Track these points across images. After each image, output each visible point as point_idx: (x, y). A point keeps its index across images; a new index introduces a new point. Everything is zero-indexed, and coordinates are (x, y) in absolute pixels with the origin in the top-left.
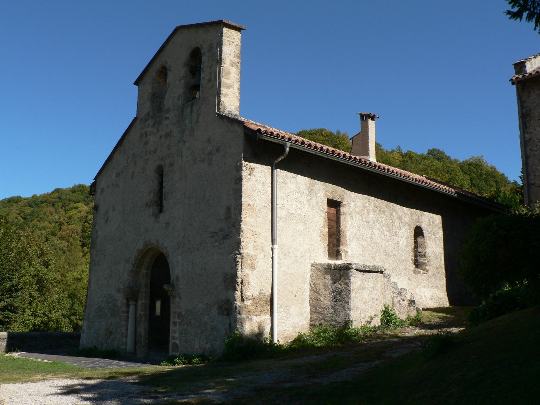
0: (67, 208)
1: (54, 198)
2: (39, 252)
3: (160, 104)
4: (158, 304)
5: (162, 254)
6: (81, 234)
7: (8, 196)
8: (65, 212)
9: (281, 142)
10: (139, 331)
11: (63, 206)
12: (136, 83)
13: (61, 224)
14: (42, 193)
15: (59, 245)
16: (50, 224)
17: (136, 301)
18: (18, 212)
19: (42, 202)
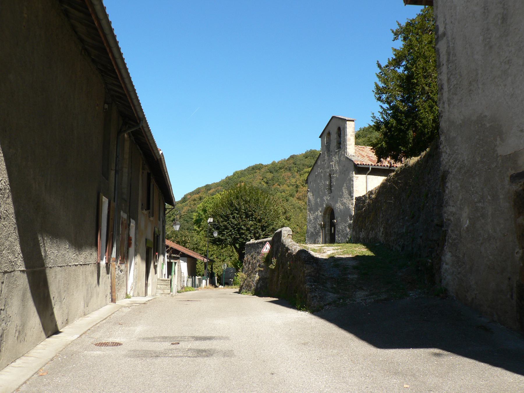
2: (284, 211)
4: (333, 228)
7: (252, 164)
9: (367, 166)
11: (298, 171)
12: (320, 137)
13: (297, 187)
14: (280, 160)
18: (261, 178)
19: (280, 168)
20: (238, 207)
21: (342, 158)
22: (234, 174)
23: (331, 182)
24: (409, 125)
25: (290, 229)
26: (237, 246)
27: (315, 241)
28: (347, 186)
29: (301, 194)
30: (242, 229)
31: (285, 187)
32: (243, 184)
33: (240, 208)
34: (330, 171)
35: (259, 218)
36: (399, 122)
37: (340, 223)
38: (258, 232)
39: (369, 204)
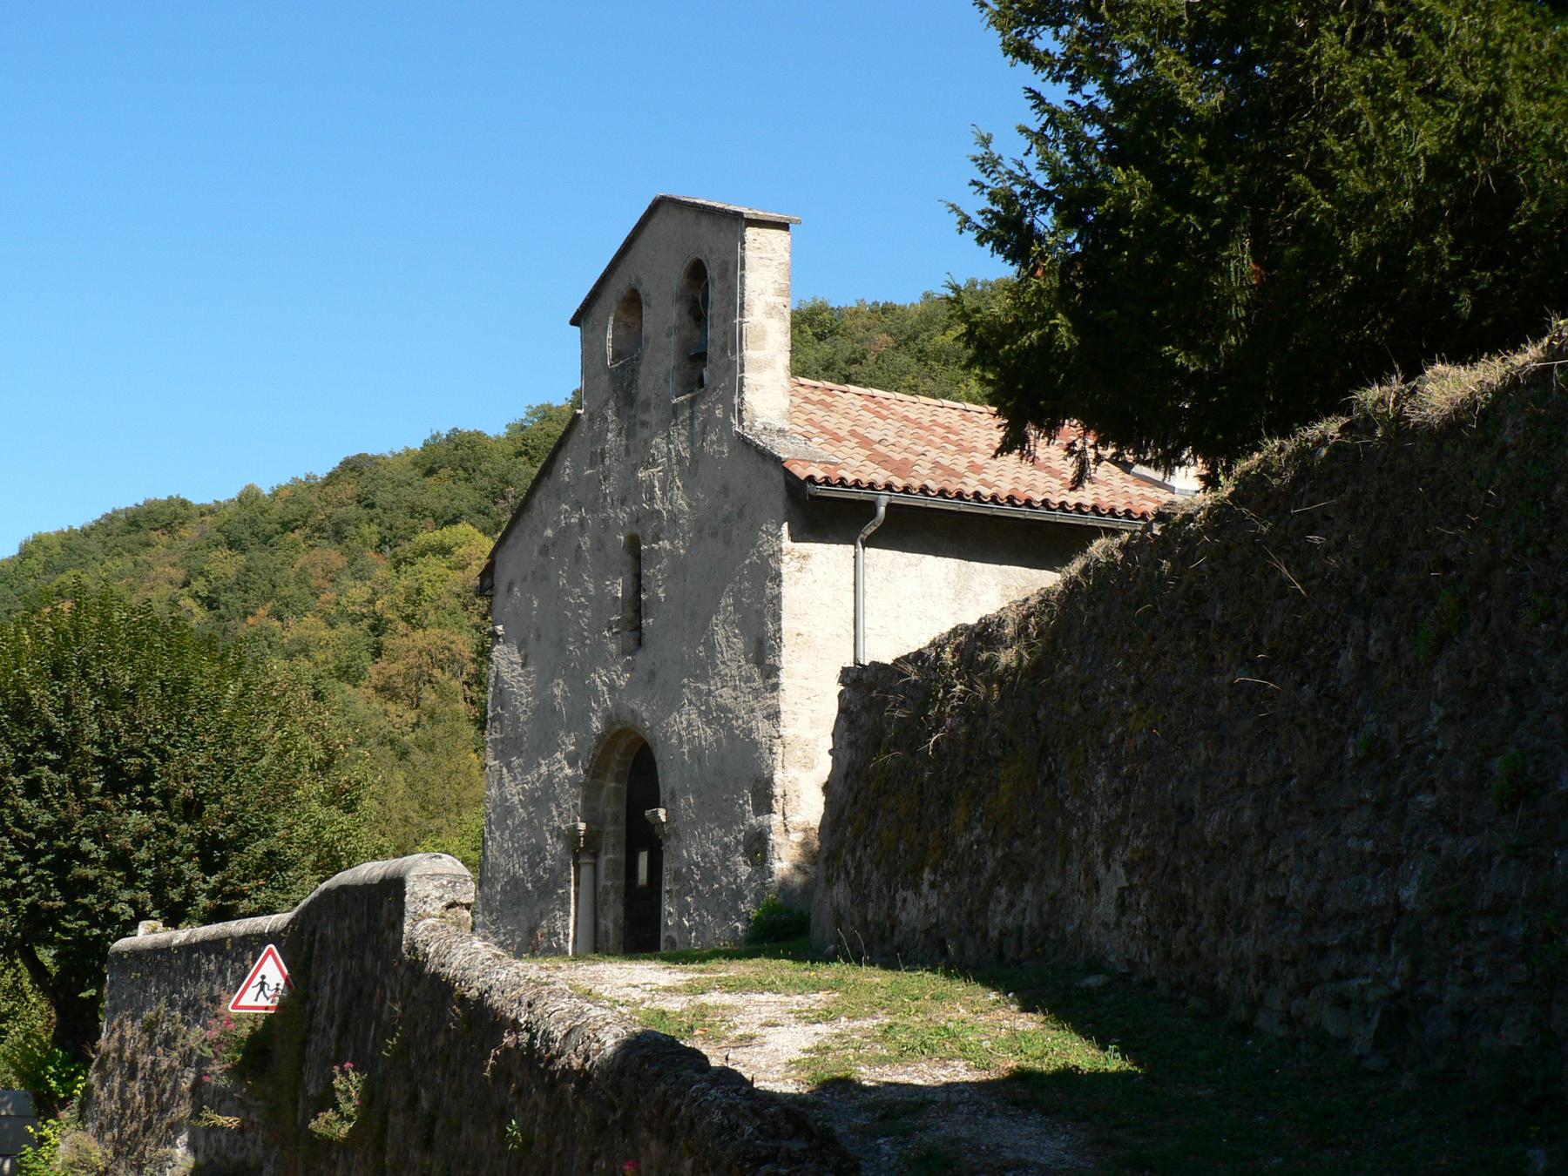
0: (406, 548)
1: (342, 504)
2: (319, 754)
3: (630, 384)
4: (643, 859)
5: (646, 744)
6: (471, 668)
7: (128, 495)
8: (397, 567)
9: (863, 495)
10: (602, 928)
11: (383, 541)
12: (575, 321)
15: (373, 723)
16: (332, 626)
17: (595, 856)
18: (179, 575)
20: (61, 727)
21: (712, 444)
22: (25, 553)
23: (637, 583)
24: (1232, 211)
25: (460, 868)
26: (46, 956)
27: (532, 931)
28: (738, 605)
29: (399, 666)
30: (85, 858)
31: (308, 626)
32: (66, 606)
33: (75, 732)
34: (637, 520)
35: (185, 791)
36: (1172, 187)
37: (694, 824)
38: (178, 879)
39: (971, 712)
